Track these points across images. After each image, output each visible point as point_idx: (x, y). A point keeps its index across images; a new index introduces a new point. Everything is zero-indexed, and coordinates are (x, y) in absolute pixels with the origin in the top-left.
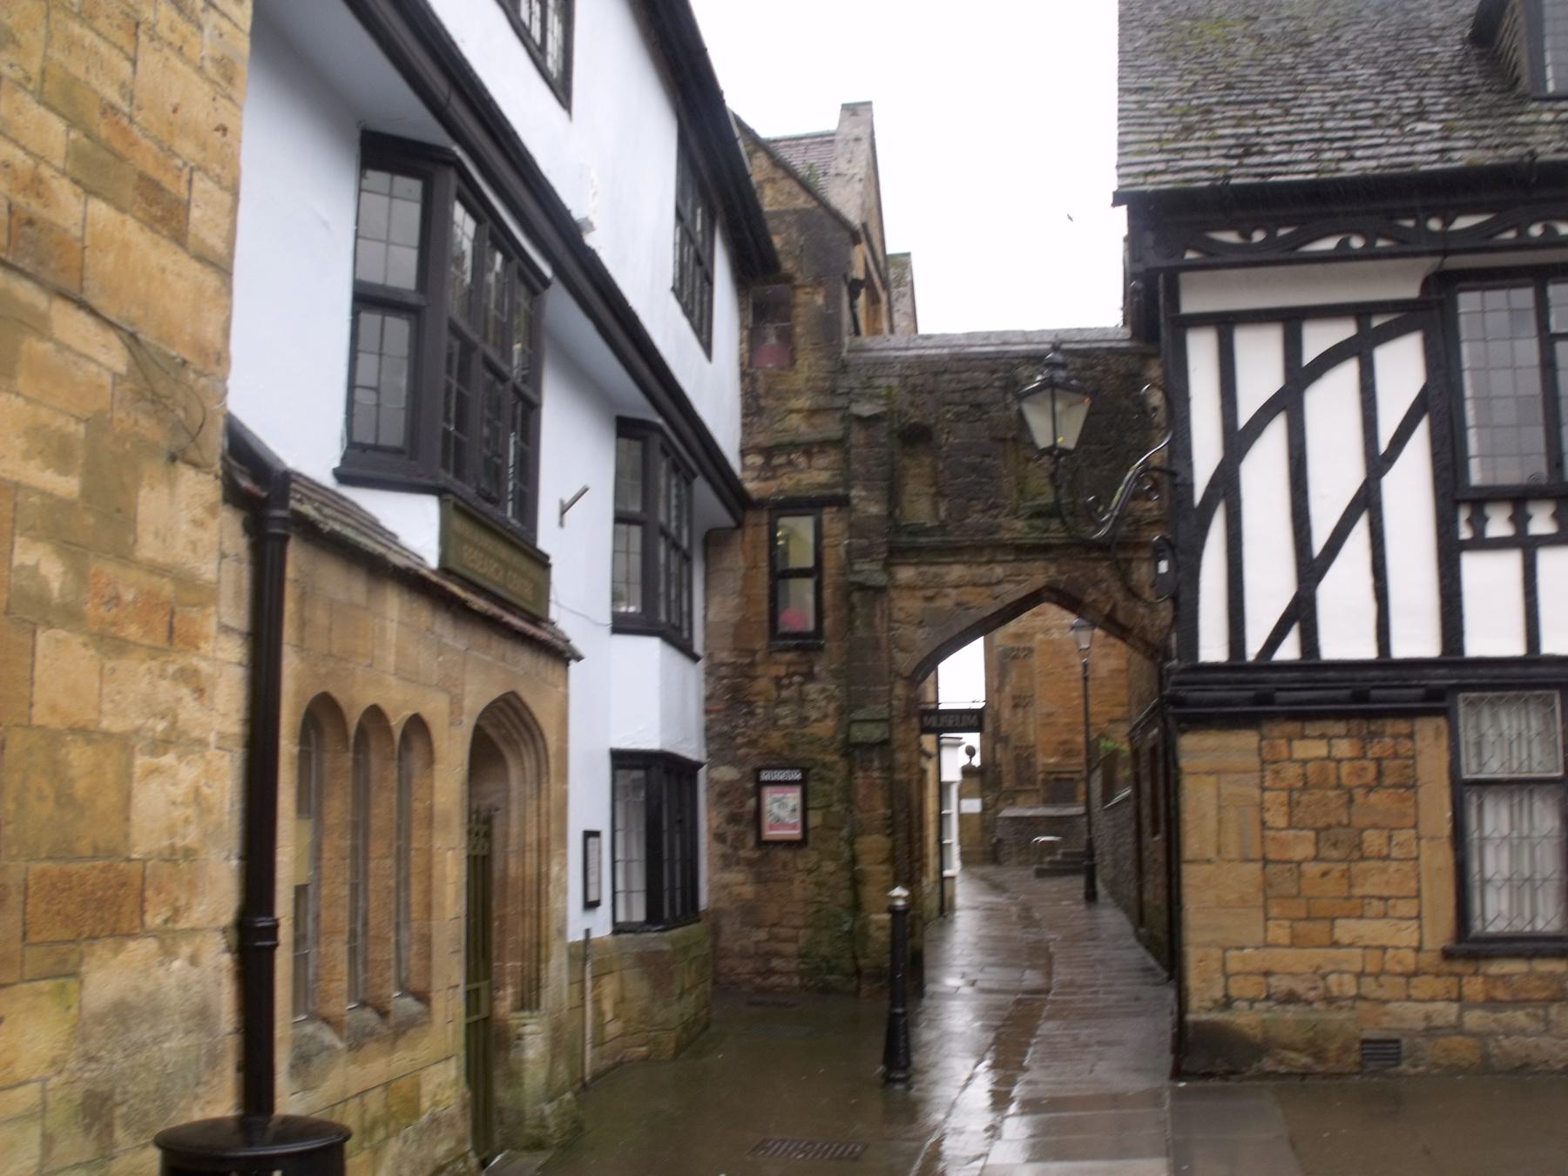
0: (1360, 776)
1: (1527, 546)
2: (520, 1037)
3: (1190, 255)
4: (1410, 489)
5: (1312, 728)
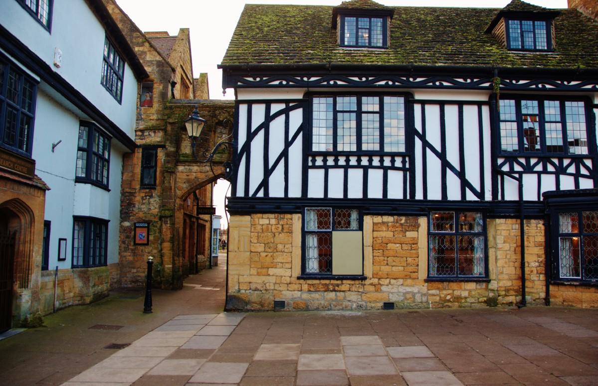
0: (277, 229)
1: (326, 168)
2: (21, 296)
3: (239, 83)
4: (296, 150)
5: (265, 216)
